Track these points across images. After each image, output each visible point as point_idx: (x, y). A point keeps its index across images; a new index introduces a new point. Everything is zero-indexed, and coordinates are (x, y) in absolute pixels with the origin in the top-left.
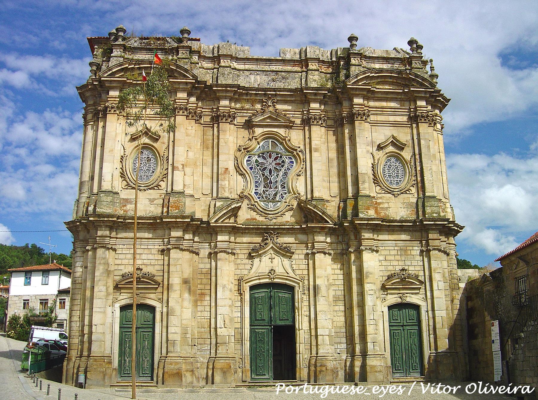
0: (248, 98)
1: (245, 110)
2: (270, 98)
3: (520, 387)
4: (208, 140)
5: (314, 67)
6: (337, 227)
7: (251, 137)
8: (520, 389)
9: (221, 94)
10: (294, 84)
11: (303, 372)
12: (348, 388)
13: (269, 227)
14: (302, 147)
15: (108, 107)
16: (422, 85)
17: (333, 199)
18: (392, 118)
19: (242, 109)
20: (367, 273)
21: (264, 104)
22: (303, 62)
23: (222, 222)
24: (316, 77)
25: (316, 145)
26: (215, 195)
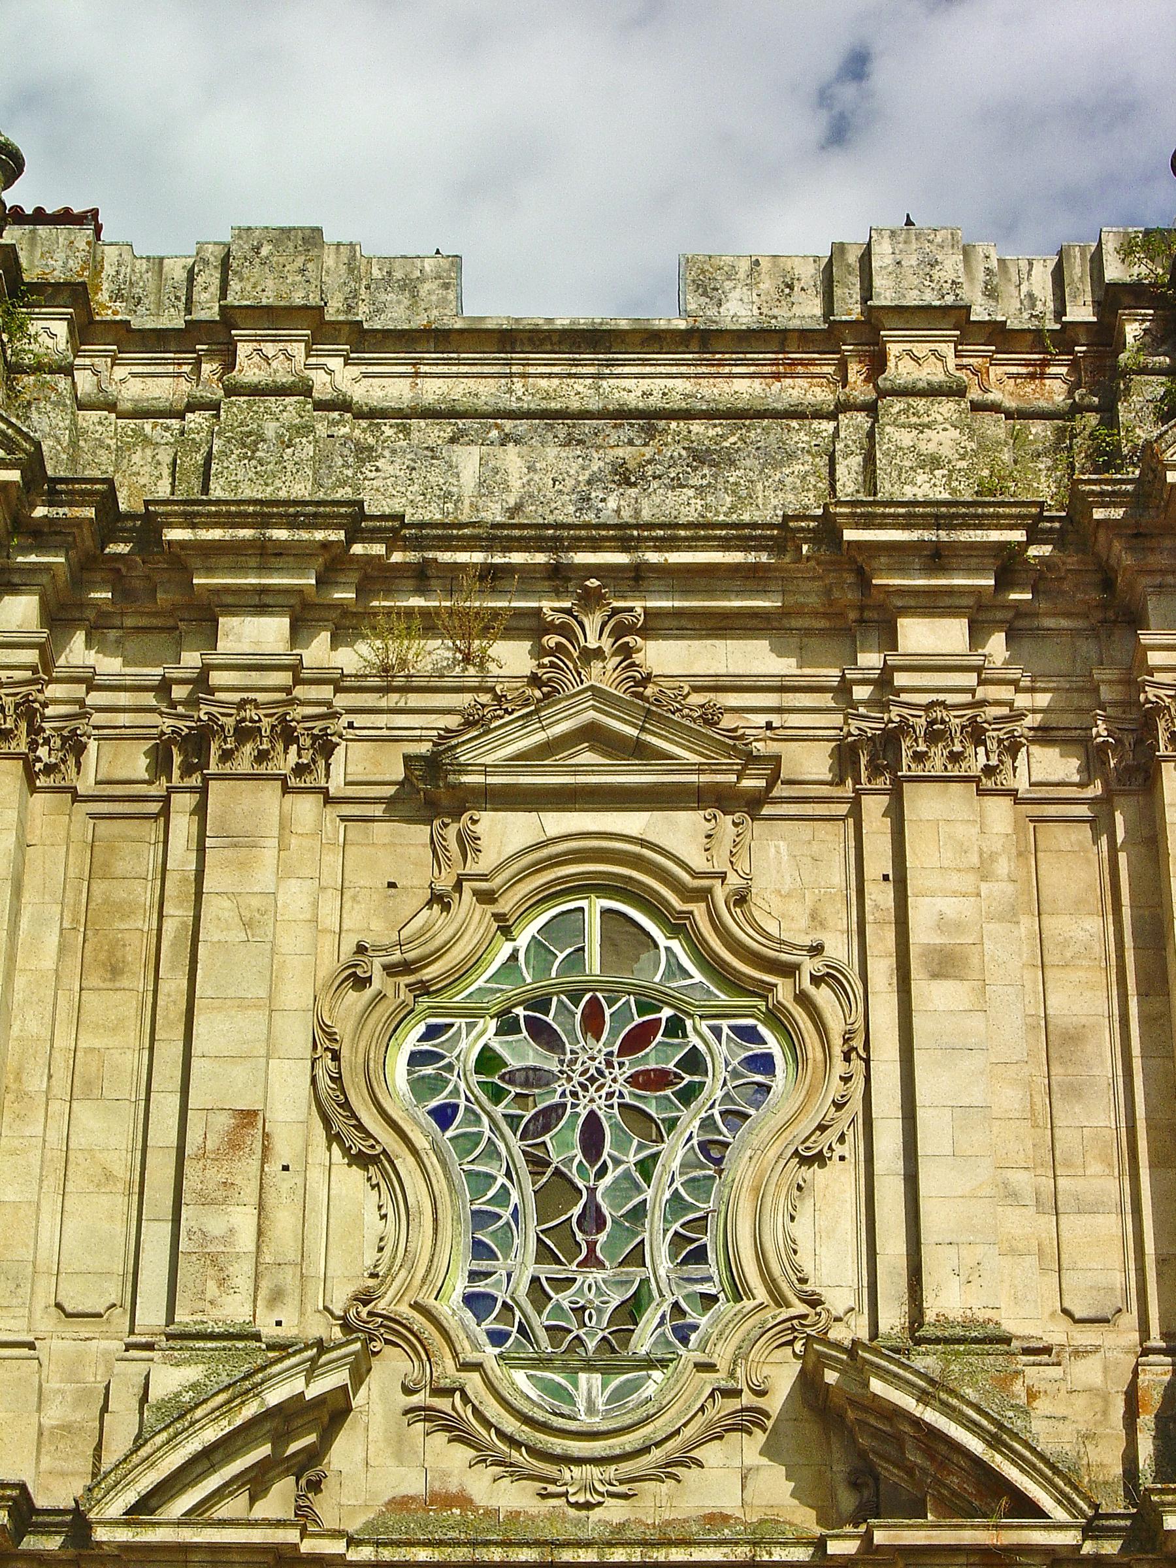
1: (392, 688)
2: (590, 600)
4: (124, 910)
5: (932, 373)
6: (1111, 1547)
7: (445, 882)
10: (779, 491)
13: (567, 1556)
14: (838, 949)
17: (1086, 1336)
19: (389, 679)
21: (551, 640)
22: (857, 336)
23: (196, 1516)
24: (944, 440)
25: (942, 924)
26: (151, 1315)
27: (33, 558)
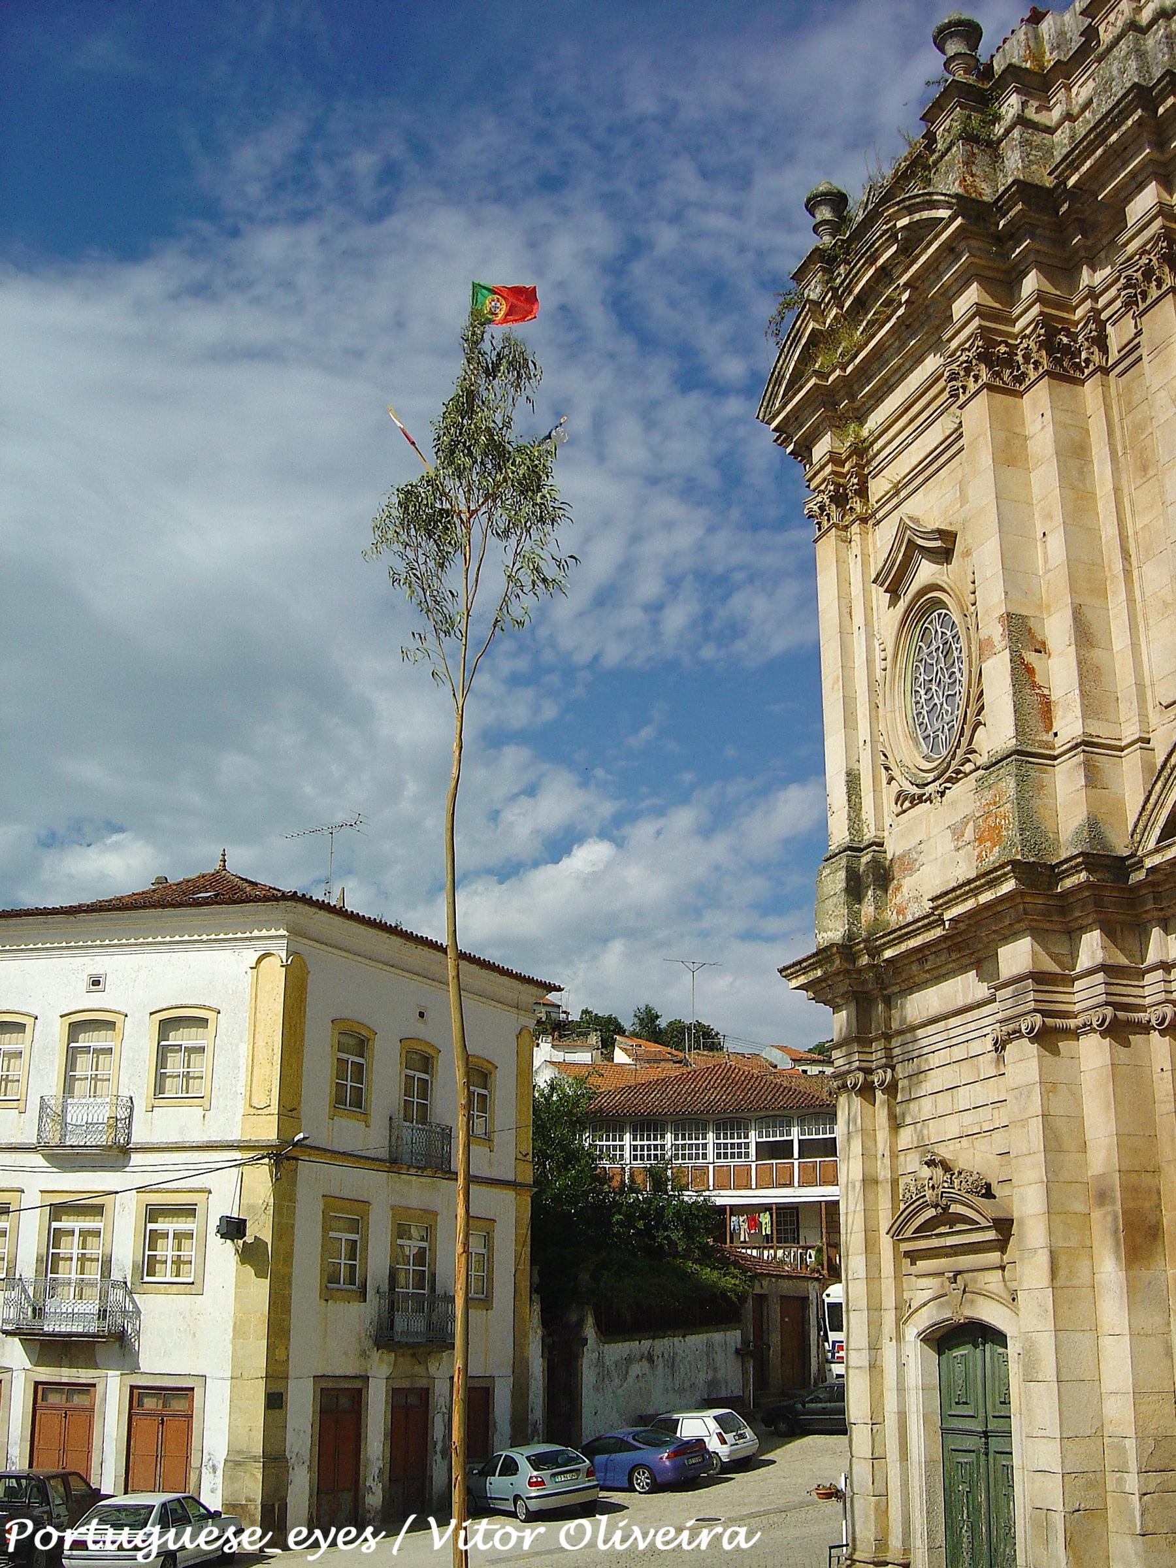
3: (719, 1529)
8: (718, 1538)
12: (216, 1533)
27: (1018, 251)
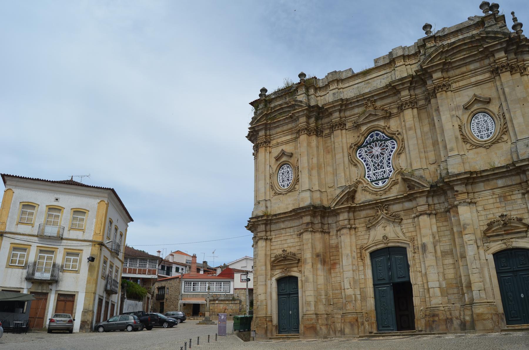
0: (353, 106)
9: (331, 110)
11: (420, 323)
15: (259, 143)
16: (495, 38)
18: (473, 80)
20: (464, 225)
